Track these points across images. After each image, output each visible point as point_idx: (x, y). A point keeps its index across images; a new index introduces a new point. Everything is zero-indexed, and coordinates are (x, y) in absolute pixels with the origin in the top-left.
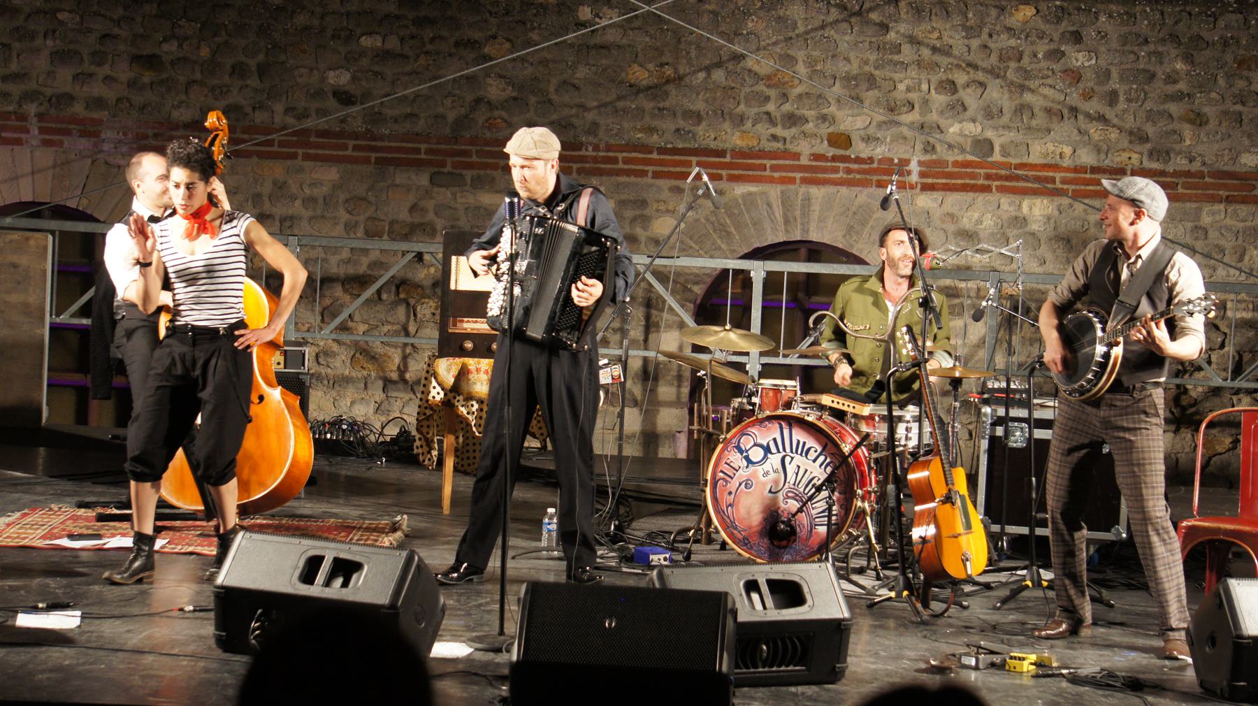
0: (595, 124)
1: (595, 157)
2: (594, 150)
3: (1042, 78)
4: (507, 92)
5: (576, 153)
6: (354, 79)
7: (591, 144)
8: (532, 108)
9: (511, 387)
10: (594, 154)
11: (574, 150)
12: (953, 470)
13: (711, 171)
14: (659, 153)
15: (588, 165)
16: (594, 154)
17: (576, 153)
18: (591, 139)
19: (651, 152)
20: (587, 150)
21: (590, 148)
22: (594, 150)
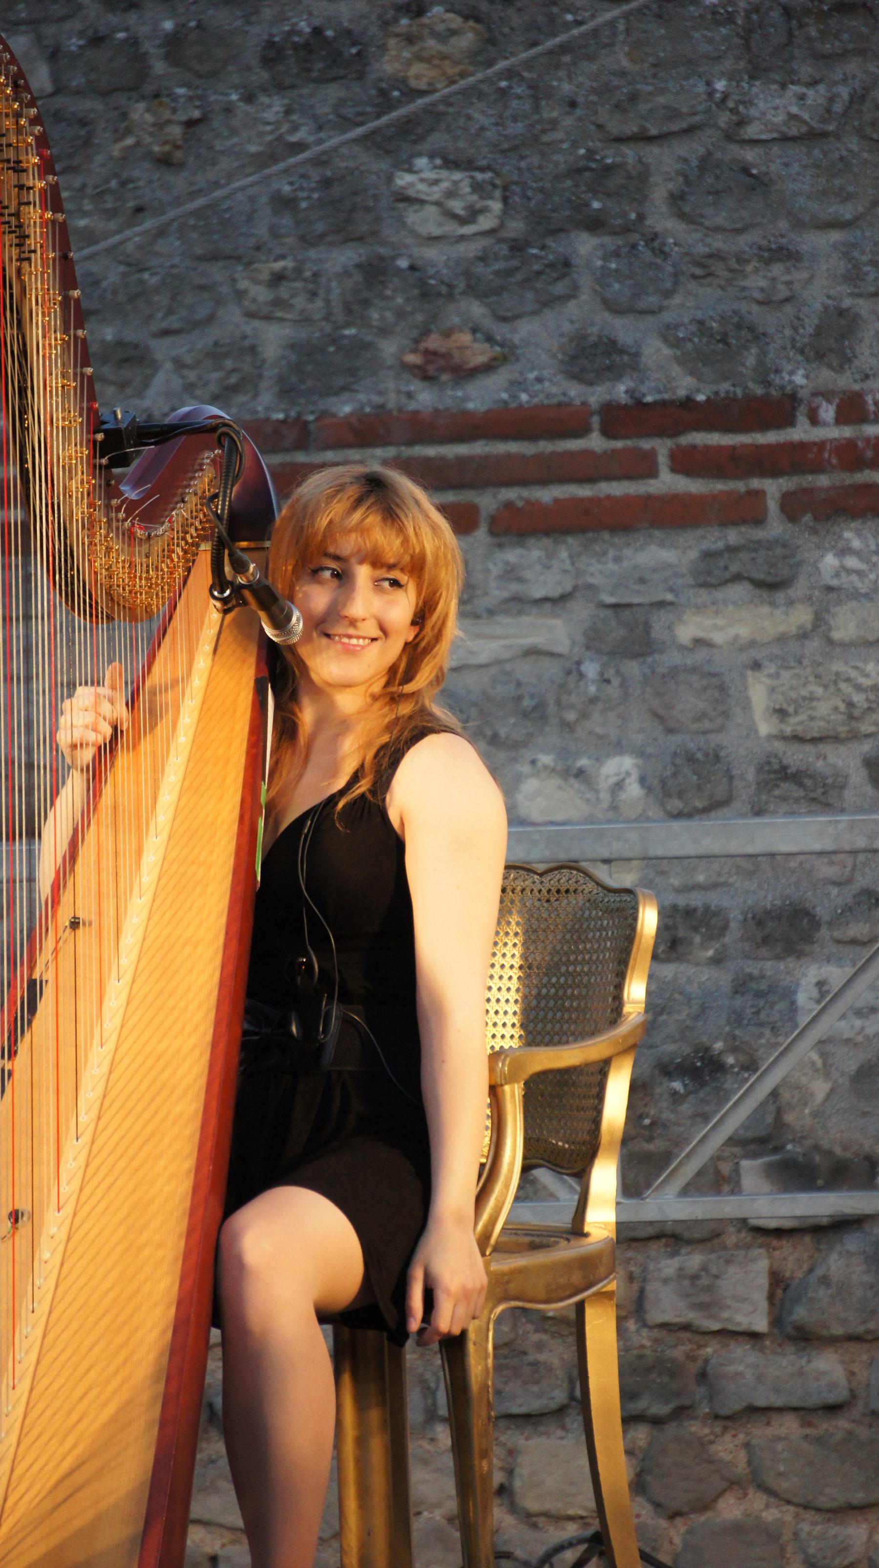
0: (842, 313)
1: (851, 444)
2: (841, 419)
3: (444, 57)
4: (486, 223)
5: (772, 437)
6: (390, 179)
7: (827, 395)
8: (585, 281)
9: (60, 985)
10: (847, 432)
11: (765, 426)
12: (694, 996)
13: (451, 497)
14: (608, 432)
15: (823, 481)
16: (847, 432)
17: (772, 437)
18: (826, 376)
19: (582, 431)
20: (814, 419)
21: (828, 412)
22: (841, 419)
